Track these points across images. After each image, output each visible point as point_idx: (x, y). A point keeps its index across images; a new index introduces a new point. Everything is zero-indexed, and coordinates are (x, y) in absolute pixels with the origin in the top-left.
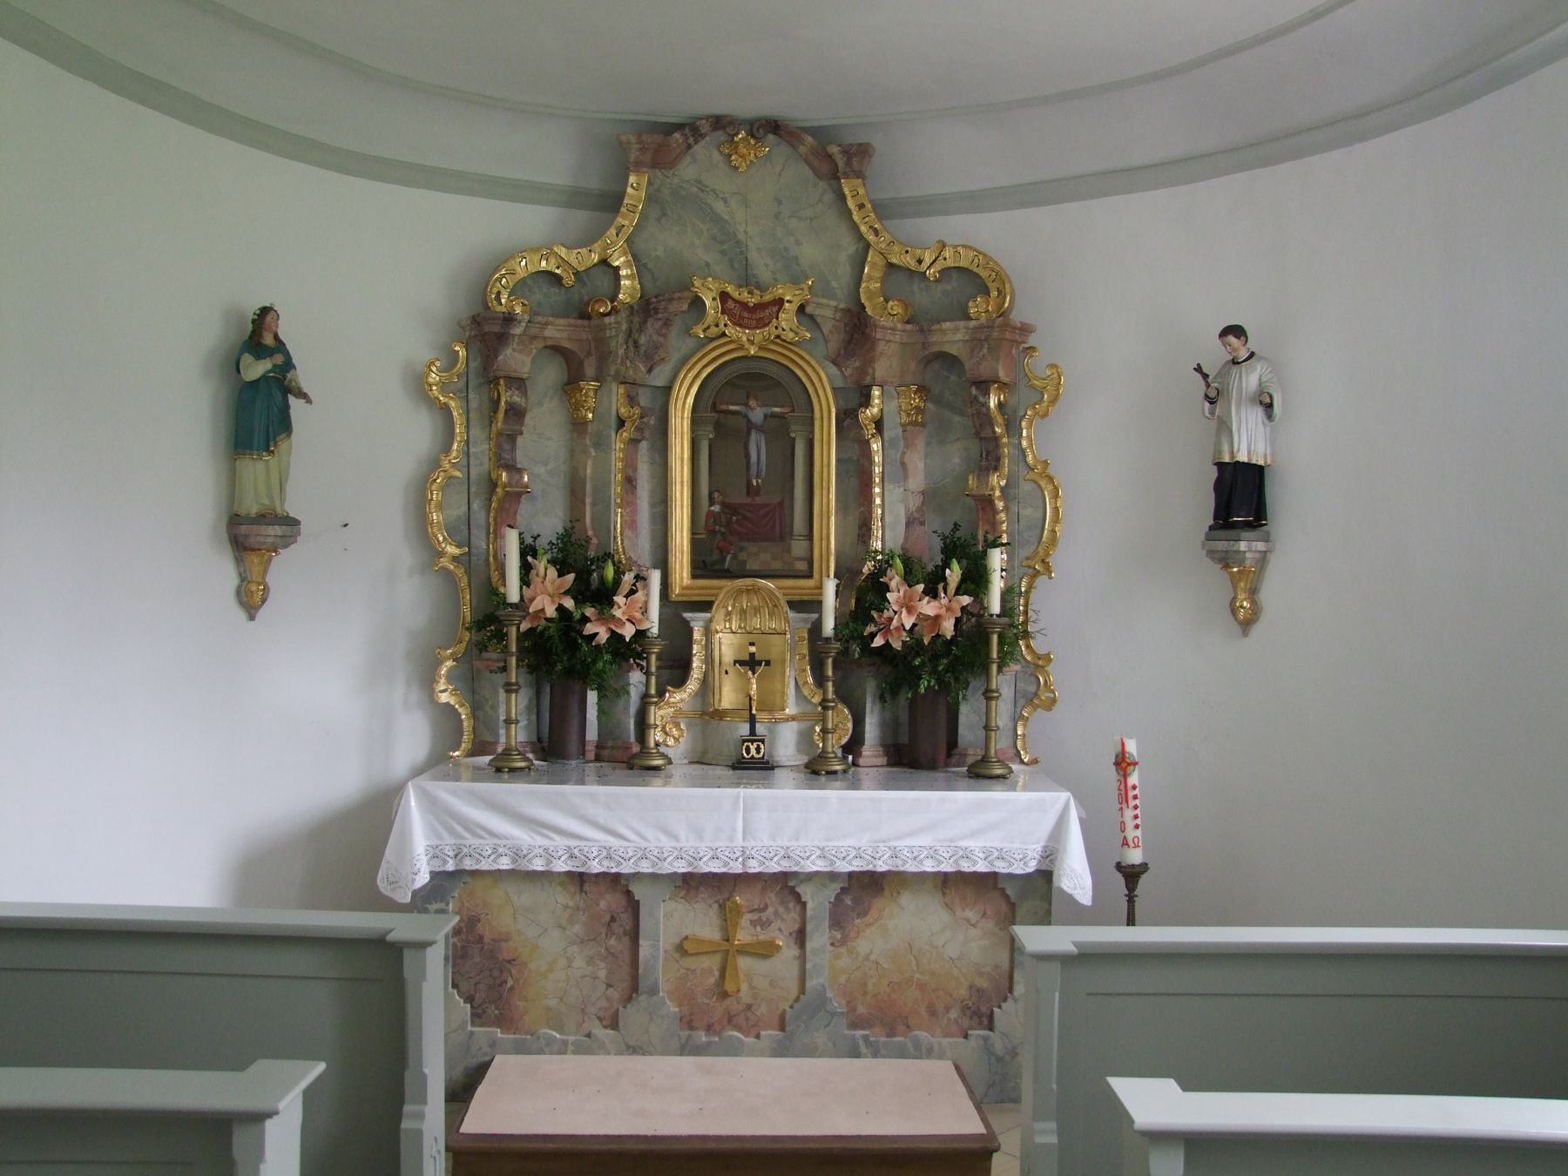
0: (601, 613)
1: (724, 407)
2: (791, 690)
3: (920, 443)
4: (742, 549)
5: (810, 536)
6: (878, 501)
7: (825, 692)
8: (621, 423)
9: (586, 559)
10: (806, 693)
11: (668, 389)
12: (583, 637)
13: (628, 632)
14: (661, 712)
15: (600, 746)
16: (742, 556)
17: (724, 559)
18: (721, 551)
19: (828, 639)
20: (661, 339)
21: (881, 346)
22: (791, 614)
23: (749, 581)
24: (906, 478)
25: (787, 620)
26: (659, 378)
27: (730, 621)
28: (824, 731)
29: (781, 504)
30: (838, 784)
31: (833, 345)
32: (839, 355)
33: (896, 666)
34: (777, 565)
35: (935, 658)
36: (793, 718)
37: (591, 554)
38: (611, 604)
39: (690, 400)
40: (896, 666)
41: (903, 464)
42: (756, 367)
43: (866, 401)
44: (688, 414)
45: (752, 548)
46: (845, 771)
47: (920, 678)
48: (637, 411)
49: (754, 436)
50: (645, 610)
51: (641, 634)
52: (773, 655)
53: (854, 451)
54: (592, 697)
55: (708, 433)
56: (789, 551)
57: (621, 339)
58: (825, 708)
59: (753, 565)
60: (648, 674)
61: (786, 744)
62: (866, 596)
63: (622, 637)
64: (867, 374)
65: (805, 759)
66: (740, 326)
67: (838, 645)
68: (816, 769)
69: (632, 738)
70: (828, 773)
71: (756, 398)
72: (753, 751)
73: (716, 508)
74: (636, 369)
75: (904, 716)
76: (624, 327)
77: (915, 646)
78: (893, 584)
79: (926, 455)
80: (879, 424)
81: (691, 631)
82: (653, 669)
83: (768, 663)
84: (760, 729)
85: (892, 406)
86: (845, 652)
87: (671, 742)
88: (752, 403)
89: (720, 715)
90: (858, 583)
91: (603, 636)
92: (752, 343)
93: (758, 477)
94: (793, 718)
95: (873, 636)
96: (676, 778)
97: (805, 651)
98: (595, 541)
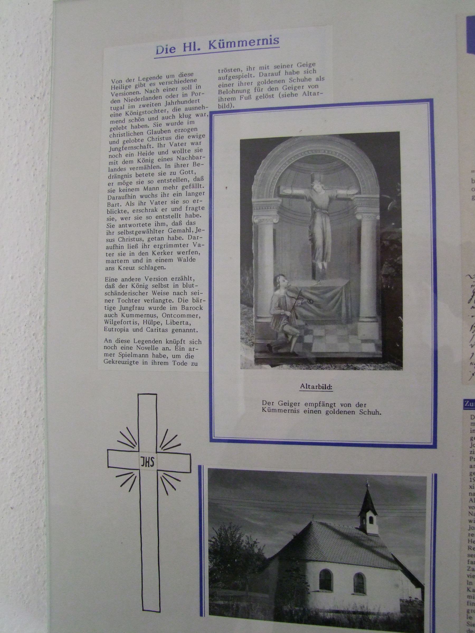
1: (288, 191)
49: (319, 220)
56: (355, 332)
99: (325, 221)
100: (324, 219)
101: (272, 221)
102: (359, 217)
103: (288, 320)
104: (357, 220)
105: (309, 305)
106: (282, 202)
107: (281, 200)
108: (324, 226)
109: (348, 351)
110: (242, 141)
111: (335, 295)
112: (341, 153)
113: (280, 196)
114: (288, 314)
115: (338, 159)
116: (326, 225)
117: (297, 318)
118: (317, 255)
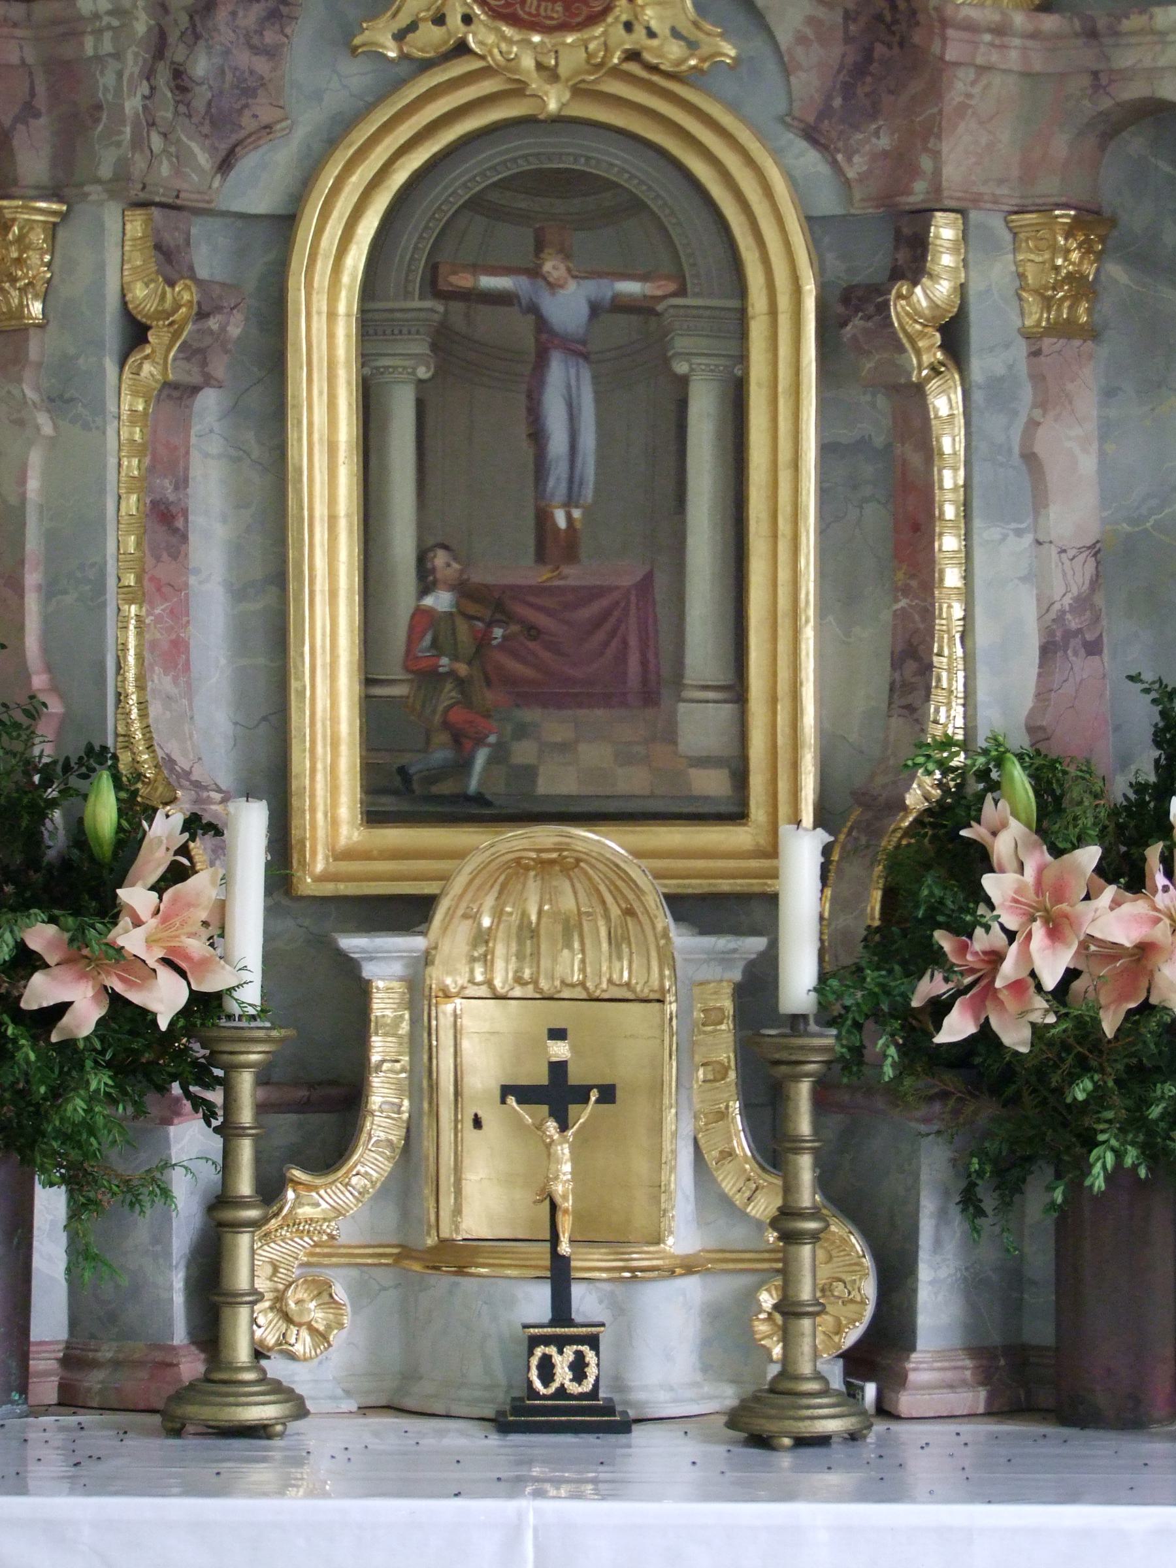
0: (78, 939)
1: (463, 281)
2: (681, 1179)
3: (1086, 401)
4: (522, 731)
5: (737, 690)
6: (952, 577)
7: (789, 1189)
8: (136, 333)
9: (29, 766)
10: (728, 1184)
11: (284, 224)
12: (20, 1016)
13: (165, 999)
14: (269, 1252)
15: (74, 1360)
16: (523, 752)
17: (463, 766)
18: (457, 738)
19: (796, 1020)
20: (261, 65)
21: (959, 86)
22: (683, 940)
23: (545, 836)
24: (1039, 500)
25: (667, 958)
26: (256, 188)
27: (487, 960)
28: (788, 1310)
29: (645, 585)
30: (833, 1479)
31: (808, 83)
32: (825, 112)
33: (1014, 1101)
34: (633, 782)
35: (1139, 1076)
36: (688, 1267)
37: (44, 750)
38: (110, 911)
39: (357, 258)
40: (1014, 1101)
41: (1030, 459)
42: (570, 154)
43: (913, 260)
44: (347, 302)
45: (555, 726)
46: (853, 1437)
47: (1090, 1143)
48: (185, 293)
49: (558, 372)
50: (218, 928)
51: (205, 1006)
52: (625, 1068)
53: (874, 419)
54: (50, 1205)
55: (412, 362)
56: (670, 736)
57: (132, 65)
58: (790, 1238)
59: (557, 781)
60: (228, 1131)
61: (665, 1347)
62: (919, 881)
63: (146, 1017)
64: (914, 172)
65: (727, 1396)
66: (514, 20)
67: (828, 1038)
68: (760, 1428)
69: (180, 1335)
70: (802, 1442)
71: (566, 254)
72: (563, 1374)
73: (440, 601)
74: (181, 159)
75: (1040, 1259)
76: (141, 25)
77: (1072, 1041)
78: (1002, 847)
79: (1106, 430)
80: (953, 334)
81: (362, 991)
82: (246, 1116)
83: (608, 1094)
84: (586, 1302)
85: (997, 274)
86: (854, 1059)
87: (302, 1343)
88: (552, 266)
89: (456, 1257)
90: (888, 842)
91: (85, 1015)
92: (550, 74)
93: (570, 502)
94: (688, 1267)
95: (939, 1008)
96: (321, 1466)
97: (725, 1053)
98: (55, 707)
99: (578, 380)
100: (573, 371)
101: (414, 373)
102: (681, 368)
103: (462, 692)
104: (675, 375)
105: (531, 645)
106: (446, 311)
107: (441, 308)
108: (574, 390)
109: (647, 792)
111: (606, 614)
112: (626, 166)
113: (438, 294)
114: (462, 669)
115: (617, 185)
116: (578, 388)
118: (551, 483)
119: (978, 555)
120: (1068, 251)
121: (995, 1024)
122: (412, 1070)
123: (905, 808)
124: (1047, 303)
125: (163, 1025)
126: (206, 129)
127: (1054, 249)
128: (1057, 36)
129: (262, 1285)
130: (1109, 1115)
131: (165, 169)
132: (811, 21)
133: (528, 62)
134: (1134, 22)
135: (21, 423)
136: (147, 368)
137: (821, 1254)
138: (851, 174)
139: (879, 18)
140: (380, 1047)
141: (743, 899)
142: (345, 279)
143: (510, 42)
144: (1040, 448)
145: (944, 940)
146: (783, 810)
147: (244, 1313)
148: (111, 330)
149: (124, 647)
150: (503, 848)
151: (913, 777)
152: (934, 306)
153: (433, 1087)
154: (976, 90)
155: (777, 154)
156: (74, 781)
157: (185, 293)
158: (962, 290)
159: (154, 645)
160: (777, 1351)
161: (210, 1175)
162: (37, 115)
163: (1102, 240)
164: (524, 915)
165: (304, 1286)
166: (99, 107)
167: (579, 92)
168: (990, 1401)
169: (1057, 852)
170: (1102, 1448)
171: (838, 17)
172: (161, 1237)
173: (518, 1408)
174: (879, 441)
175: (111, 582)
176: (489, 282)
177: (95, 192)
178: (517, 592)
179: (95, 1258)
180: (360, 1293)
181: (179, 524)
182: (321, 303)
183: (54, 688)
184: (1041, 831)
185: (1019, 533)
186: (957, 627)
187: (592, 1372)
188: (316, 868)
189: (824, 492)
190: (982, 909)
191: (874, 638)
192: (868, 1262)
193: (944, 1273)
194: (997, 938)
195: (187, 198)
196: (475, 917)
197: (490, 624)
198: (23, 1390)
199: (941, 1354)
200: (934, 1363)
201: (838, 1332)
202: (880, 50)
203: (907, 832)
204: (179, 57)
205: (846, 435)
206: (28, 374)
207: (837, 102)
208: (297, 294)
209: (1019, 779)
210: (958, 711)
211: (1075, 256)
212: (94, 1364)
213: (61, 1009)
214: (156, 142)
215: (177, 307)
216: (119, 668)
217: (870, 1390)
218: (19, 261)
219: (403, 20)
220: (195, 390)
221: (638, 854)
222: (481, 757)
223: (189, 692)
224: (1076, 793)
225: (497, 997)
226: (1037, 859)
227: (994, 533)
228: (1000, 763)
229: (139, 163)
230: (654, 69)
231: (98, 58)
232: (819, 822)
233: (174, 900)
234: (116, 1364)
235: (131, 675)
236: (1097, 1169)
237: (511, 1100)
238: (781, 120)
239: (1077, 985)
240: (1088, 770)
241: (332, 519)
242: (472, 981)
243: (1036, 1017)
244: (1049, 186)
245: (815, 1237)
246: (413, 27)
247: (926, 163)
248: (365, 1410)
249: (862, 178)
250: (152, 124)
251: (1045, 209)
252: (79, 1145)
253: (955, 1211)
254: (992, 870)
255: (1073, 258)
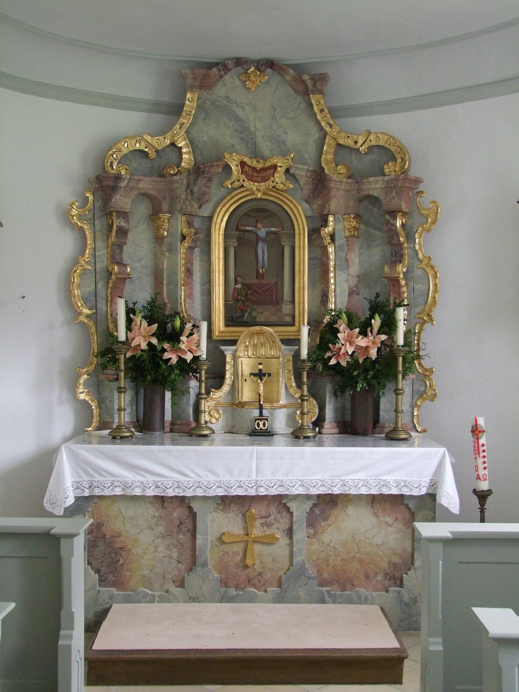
0: (173, 346)
1: (243, 228)
2: (283, 390)
4: (254, 310)
5: (293, 302)
6: (332, 281)
7: (302, 391)
8: (184, 238)
11: (210, 218)
13: (189, 357)
14: (208, 404)
15: (172, 424)
16: (254, 314)
19: (304, 361)
20: (206, 189)
21: (333, 192)
22: (283, 347)
23: (258, 328)
25: (280, 350)
26: (205, 212)
27: (247, 351)
28: (302, 413)
31: (306, 192)
33: (344, 375)
34: (274, 319)
35: (366, 371)
36: (284, 406)
37: (167, 313)
39: (224, 224)
40: (344, 375)
41: (347, 260)
42: (262, 205)
43: (325, 223)
44: (222, 232)
46: (314, 437)
47: (357, 382)
48: (193, 230)
49: (260, 244)
50: (198, 345)
51: (196, 359)
52: (273, 371)
53: (318, 252)
54: (168, 395)
55: (233, 243)
56: (281, 310)
57: (183, 189)
58: (303, 400)
60: (200, 381)
61: (280, 421)
63: (185, 360)
64: (325, 208)
65: (291, 430)
66: (252, 181)
67: (310, 364)
68: (298, 435)
69: (191, 419)
70: (305, 437)
71: (261, 223)
72: (261, 426)
73: (239, 286)
74: (192, 206)
75: (348, 405)
77: (354, 364)
78: (341, 329)
79: (360, 255)
80: (332, 237)
81: (225, 357)
82: (203, 379)
84: (265, 413)
85: (341, 226)
86: (314, 368)
87: (214, 421)
88: (259, 225)
89: (242, 405)
90: (321, 329)
91: (174, 360)
92: (259, 190)
94: (284, 406)
95: (330, 358)
97: (291, 368)
98: (169, 305)
102: (283, 244)
110: (401, 683)
114: (243, 298)
117: (248, 301)
119: (337, 276)
120: (353, 222)
121: (340, 361)
122: (234, 371)
123: (323, 323)
124: (350, 231)
125: (188, 362)
126: (197, 201)
127: (351, 221)
128: (351, 183)
129: (206, 410)
130: (361, 377)
131: (189, 208)
132: (306, 181)
133: (255, 188)
134: (365, 180)
135: (163, 254)
136: (186, 244)
137: (308, 404)
138: (314, 208)
139: (319, 180)
140: (228, 367)
141: (295, 340)
142: (222, 228)
143: (251, 184)
144: (348, 258)
145: (331, 346)
146: (301, 323)
147: (203, 414)
148: (179, 237)
149: (182, 294)
150: (251, 330)
151: (325, 317)
152: (329, 232)
153: (238, 374)
154: (336, 193)
155: (300, 205)
156: (172, 318)
157: (193, 230)
158: (334, 229)
159: (187, 294)
160: (300, 422)
161: (197, 390)
162: (166, 198)
163: (360, 220)
164: (254, 342)
165: (214, 410)
166: (177, 197)
167: (264, 194)
168: (339, 431)
169: (351, 330)
170: (360, 438)
171: (311, 180)
172: (188, 401)
173: (253, 432)
174: (319, 257)
175: (179, 283)
176: (247, 228)
177: (176, 212)
178: (253, 284)
179: (176, 404)
180: (224, 412)
181: (191, 272)
182: (217, 232)
183: (169, 302)
184: (348, 326)
185: (344, 273)
186: (333, 290)
187: (267, 425)
188: (216, 334)
189: (309, 266)
190: (338, 340)
191: (318, 293)
192: (317, 405)
193: (330, 407)
194: (340, 345)
195: (193, 213)
196: (245, 343)
197: (248, 290)
198: (163, 429)
199: (330, 422)
200: (329, 425)
201: (311, 418)
202: (319, 186)
203: (324, 327)
204: (192, 188)
205: (313, 256)
206: (164, 246)
207: (311, 195)
208: (213, 231)
209: (344, 316)
210: (333, 305)
211: (355, 223)
212: (176, 424)
213: (170, 359)
214: (188, 203)
215: (191, 233)
216: (181, 298)
217: (317, 429)
218: (163, 225)
219: (232, 181)
220: (194, 248)
221: (276, 332)
222: (246, 314)
223: (193, 302)
224: (355, 319)
225: (249, 357)
226: (347, 331)
227: (340, 273)
228: (341, 313)
229: (184, 207)
230: (278, 189)
231: (177, 188)
232: (308, 324)
233: (190, 339)
234: (180, 424)
235: (183, 299)
236: (359, 387)
237: (252, 376)
238: (301, 198)
239: (355, 354)
240: (357, 314)
241: (219, 271)
242: (244, 354)
243: (347, 360)
244: (350, 210)
245: (307, 400)
246: (234, 182)
247: (327, 206)
248: (225, 433)
249: (316, 209)
250: (187, 200)
251: (349, 214)
252: (173, 384)
253: (333, 396)
254: (339, 333)
255: (354, 223)
